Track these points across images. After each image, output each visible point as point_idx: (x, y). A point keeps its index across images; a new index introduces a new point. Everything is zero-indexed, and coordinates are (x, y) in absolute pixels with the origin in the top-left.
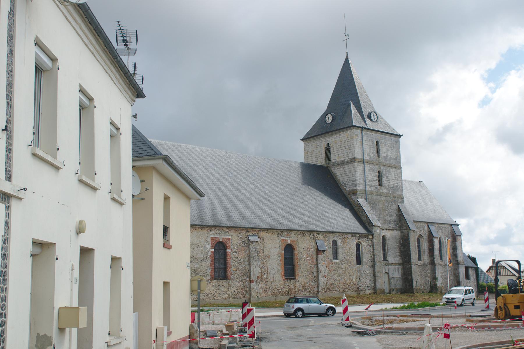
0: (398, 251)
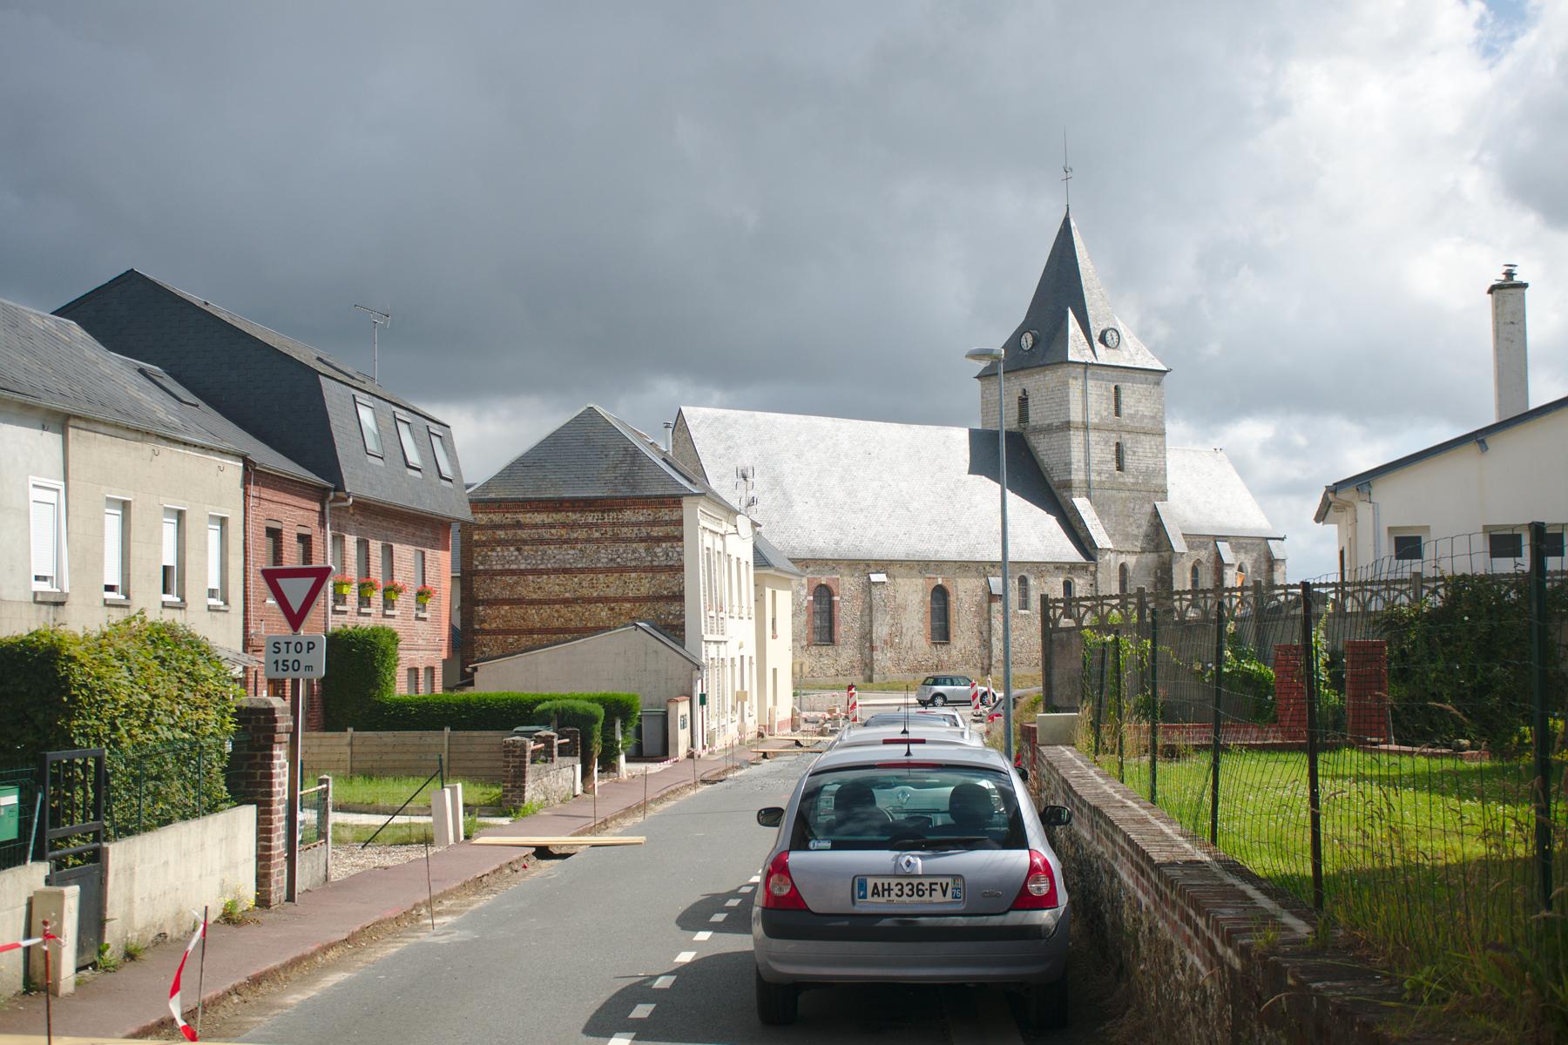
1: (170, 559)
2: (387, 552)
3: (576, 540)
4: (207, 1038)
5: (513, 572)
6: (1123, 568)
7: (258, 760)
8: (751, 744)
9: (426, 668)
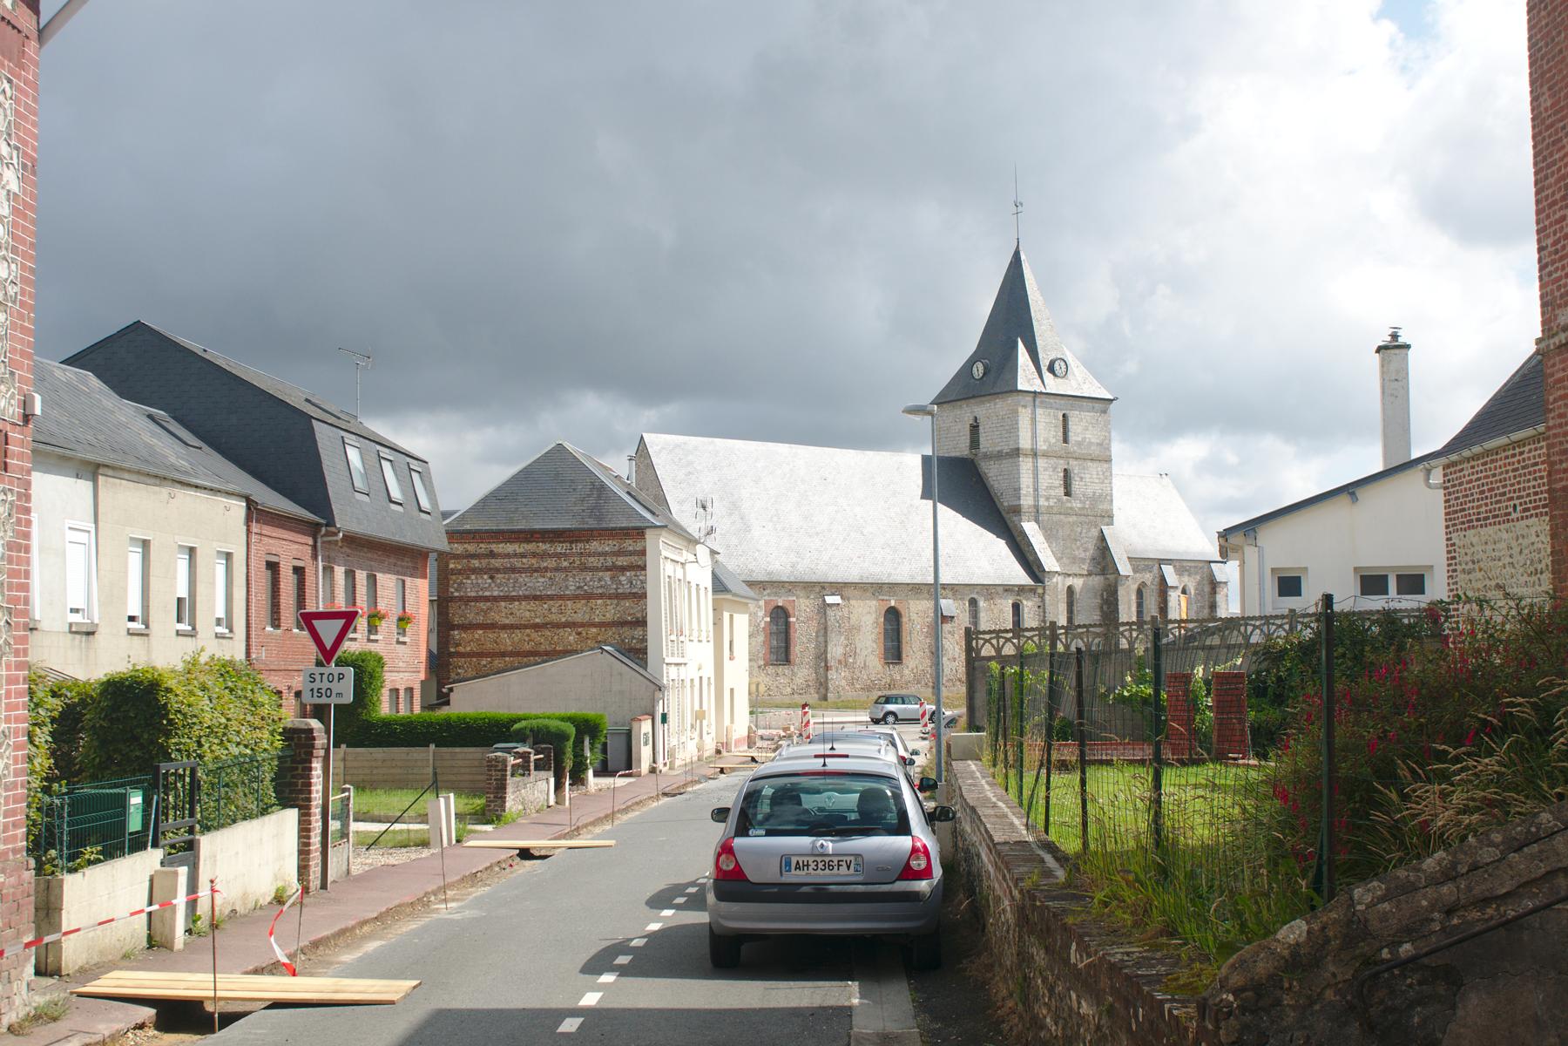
0: (1098, 613)
1: (183, 592)
2: (371, 581)
3: (546, 569)
4: (304, 975)
5: (486, 599)
6: (1070, 590)
7: (300, 771)
8: (709, 761)
9: (406, 689)
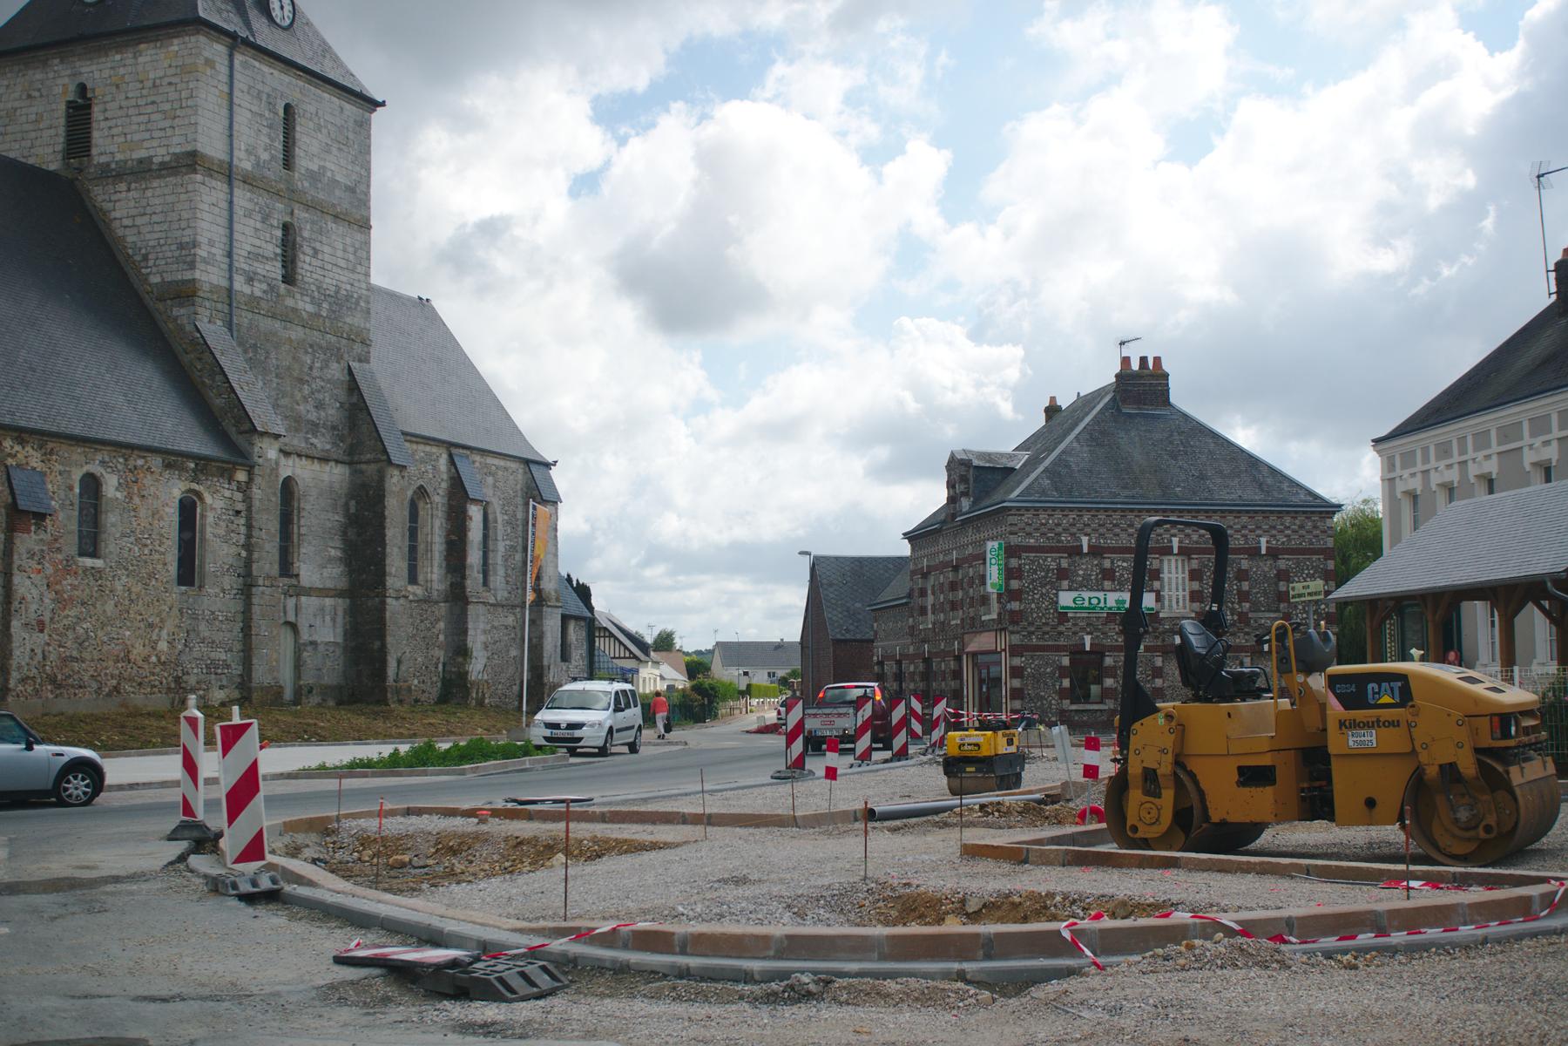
0: (338, 544)
